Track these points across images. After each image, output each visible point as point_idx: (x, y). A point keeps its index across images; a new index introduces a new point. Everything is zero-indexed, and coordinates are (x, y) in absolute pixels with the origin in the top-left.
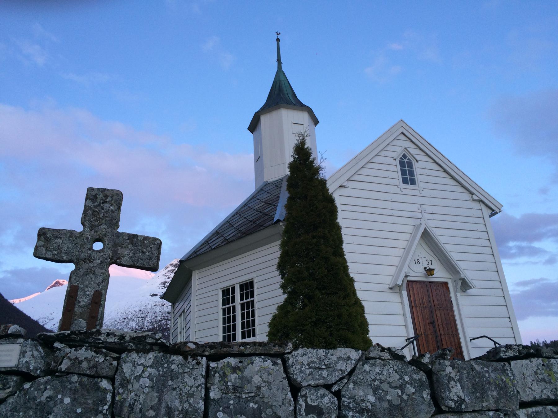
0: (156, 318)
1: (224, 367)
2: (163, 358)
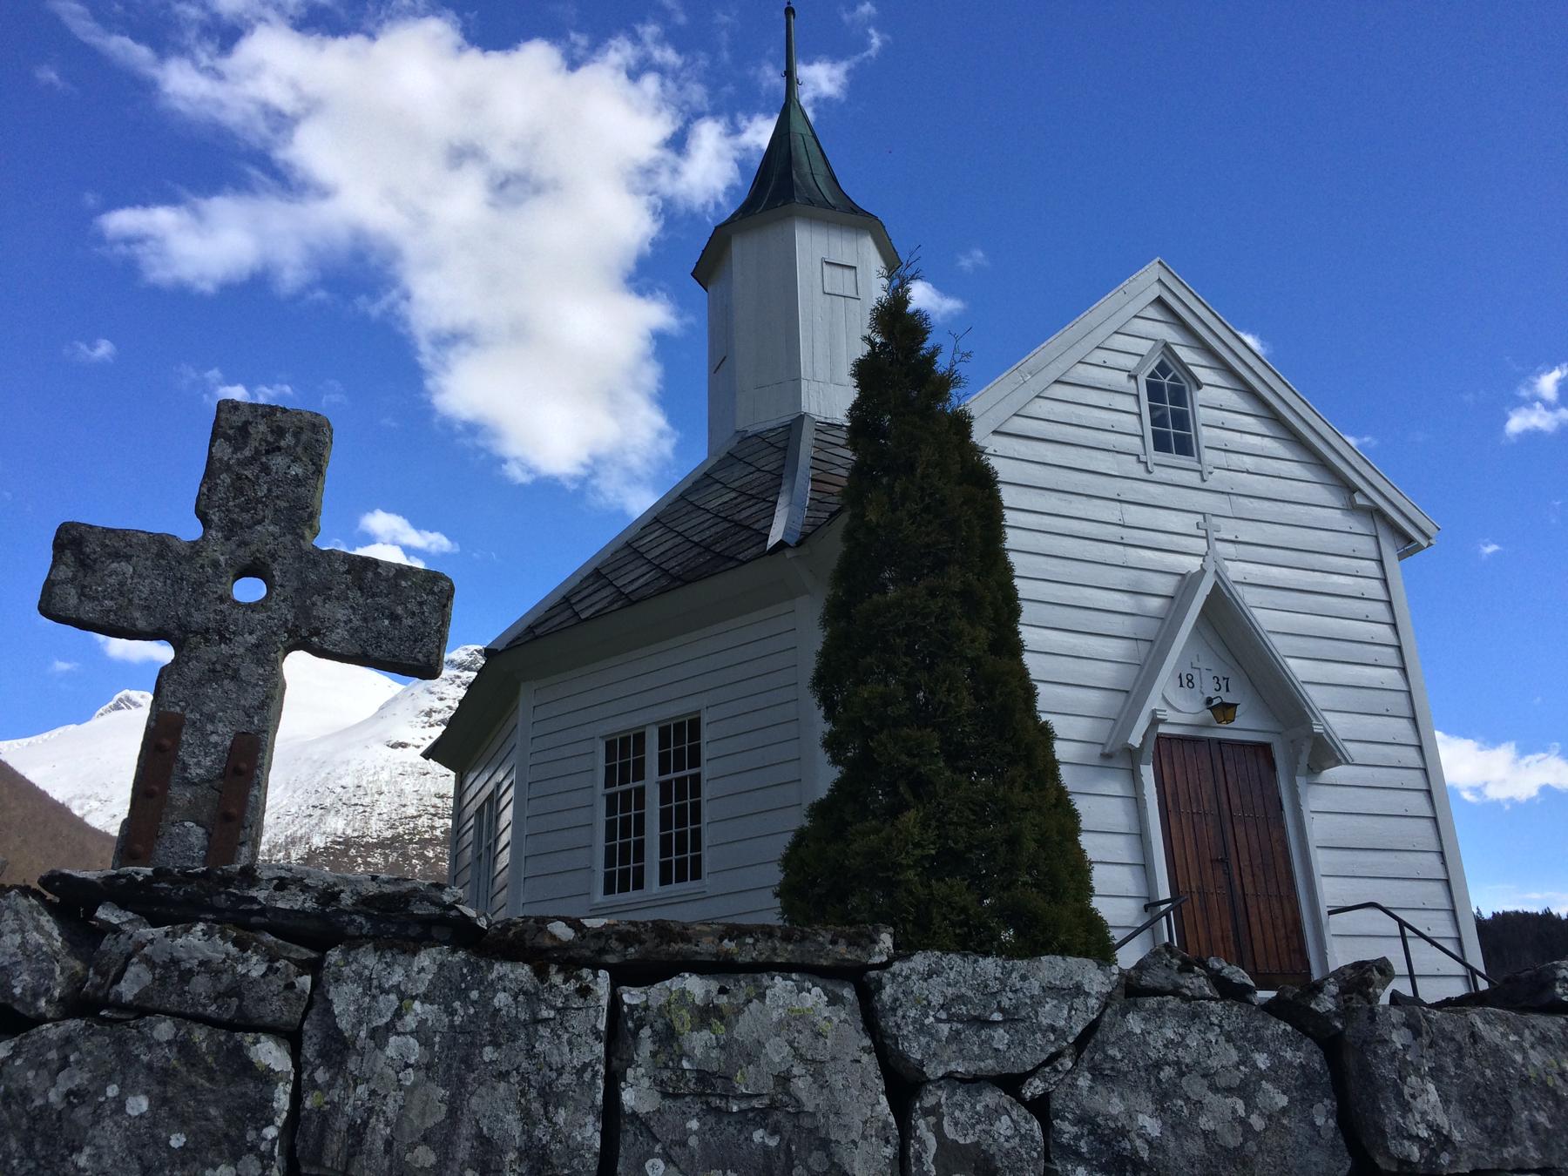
0: (403, 809)
1: (669, 1006)
2: (465, 971)
